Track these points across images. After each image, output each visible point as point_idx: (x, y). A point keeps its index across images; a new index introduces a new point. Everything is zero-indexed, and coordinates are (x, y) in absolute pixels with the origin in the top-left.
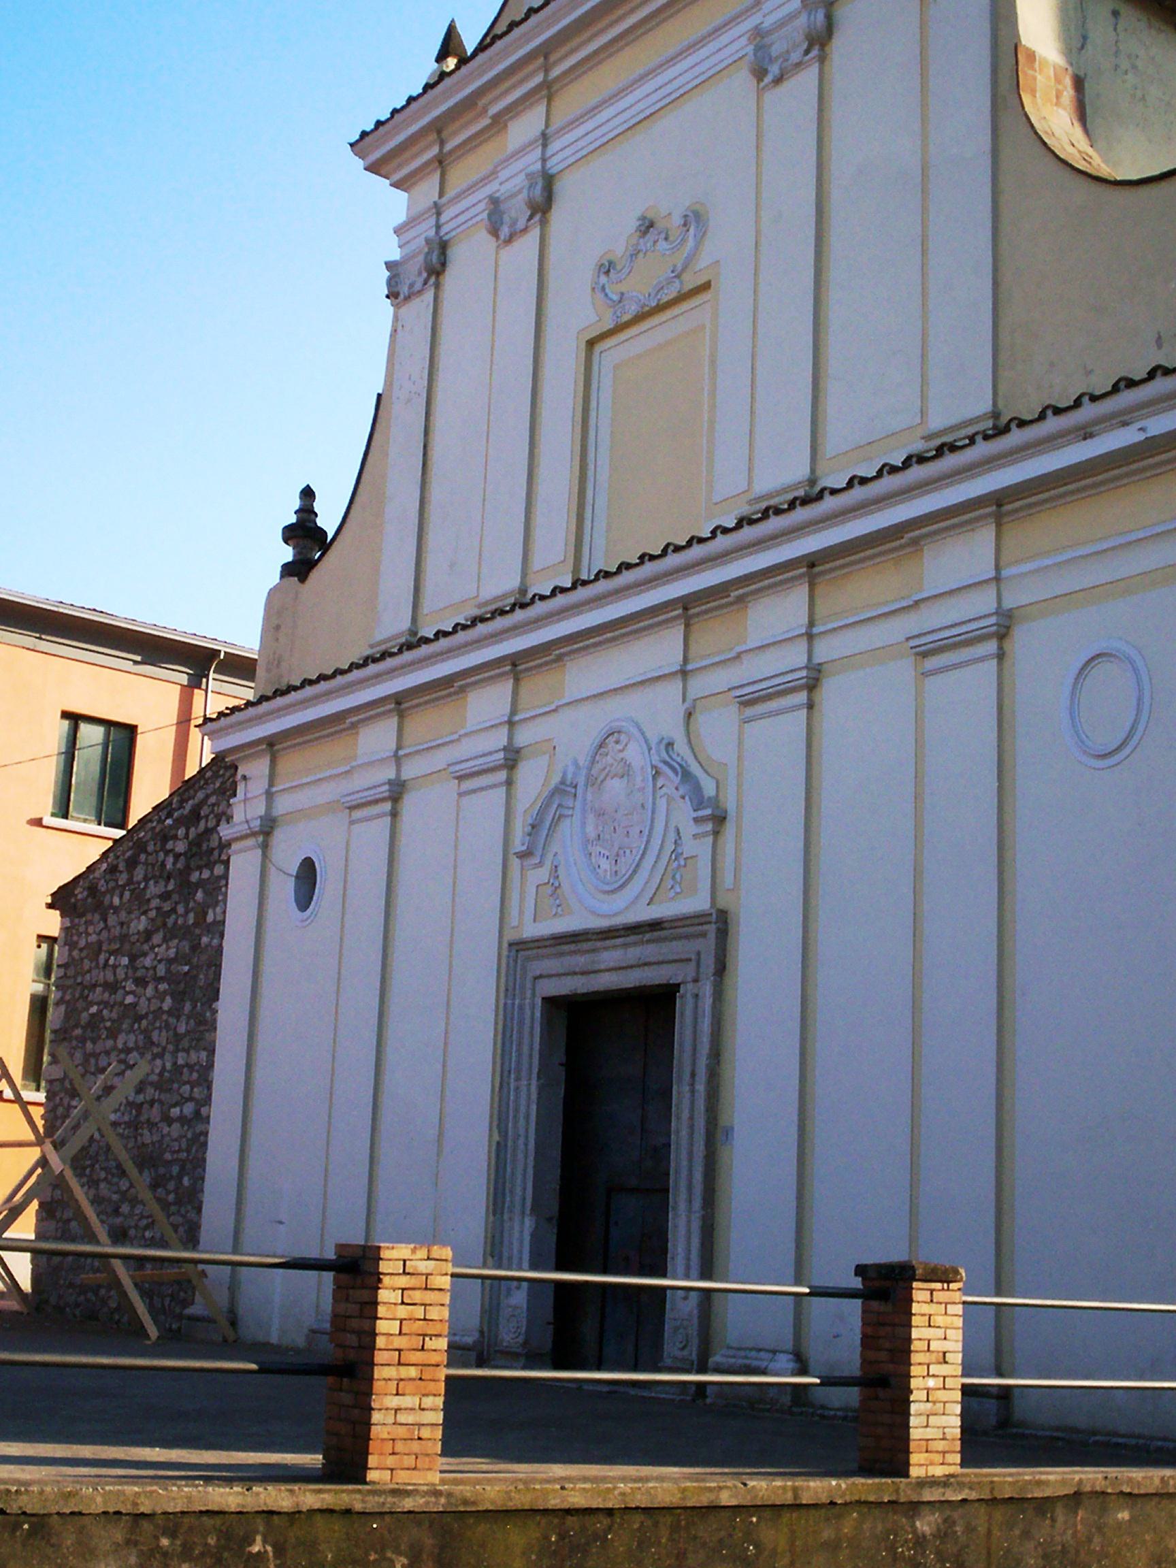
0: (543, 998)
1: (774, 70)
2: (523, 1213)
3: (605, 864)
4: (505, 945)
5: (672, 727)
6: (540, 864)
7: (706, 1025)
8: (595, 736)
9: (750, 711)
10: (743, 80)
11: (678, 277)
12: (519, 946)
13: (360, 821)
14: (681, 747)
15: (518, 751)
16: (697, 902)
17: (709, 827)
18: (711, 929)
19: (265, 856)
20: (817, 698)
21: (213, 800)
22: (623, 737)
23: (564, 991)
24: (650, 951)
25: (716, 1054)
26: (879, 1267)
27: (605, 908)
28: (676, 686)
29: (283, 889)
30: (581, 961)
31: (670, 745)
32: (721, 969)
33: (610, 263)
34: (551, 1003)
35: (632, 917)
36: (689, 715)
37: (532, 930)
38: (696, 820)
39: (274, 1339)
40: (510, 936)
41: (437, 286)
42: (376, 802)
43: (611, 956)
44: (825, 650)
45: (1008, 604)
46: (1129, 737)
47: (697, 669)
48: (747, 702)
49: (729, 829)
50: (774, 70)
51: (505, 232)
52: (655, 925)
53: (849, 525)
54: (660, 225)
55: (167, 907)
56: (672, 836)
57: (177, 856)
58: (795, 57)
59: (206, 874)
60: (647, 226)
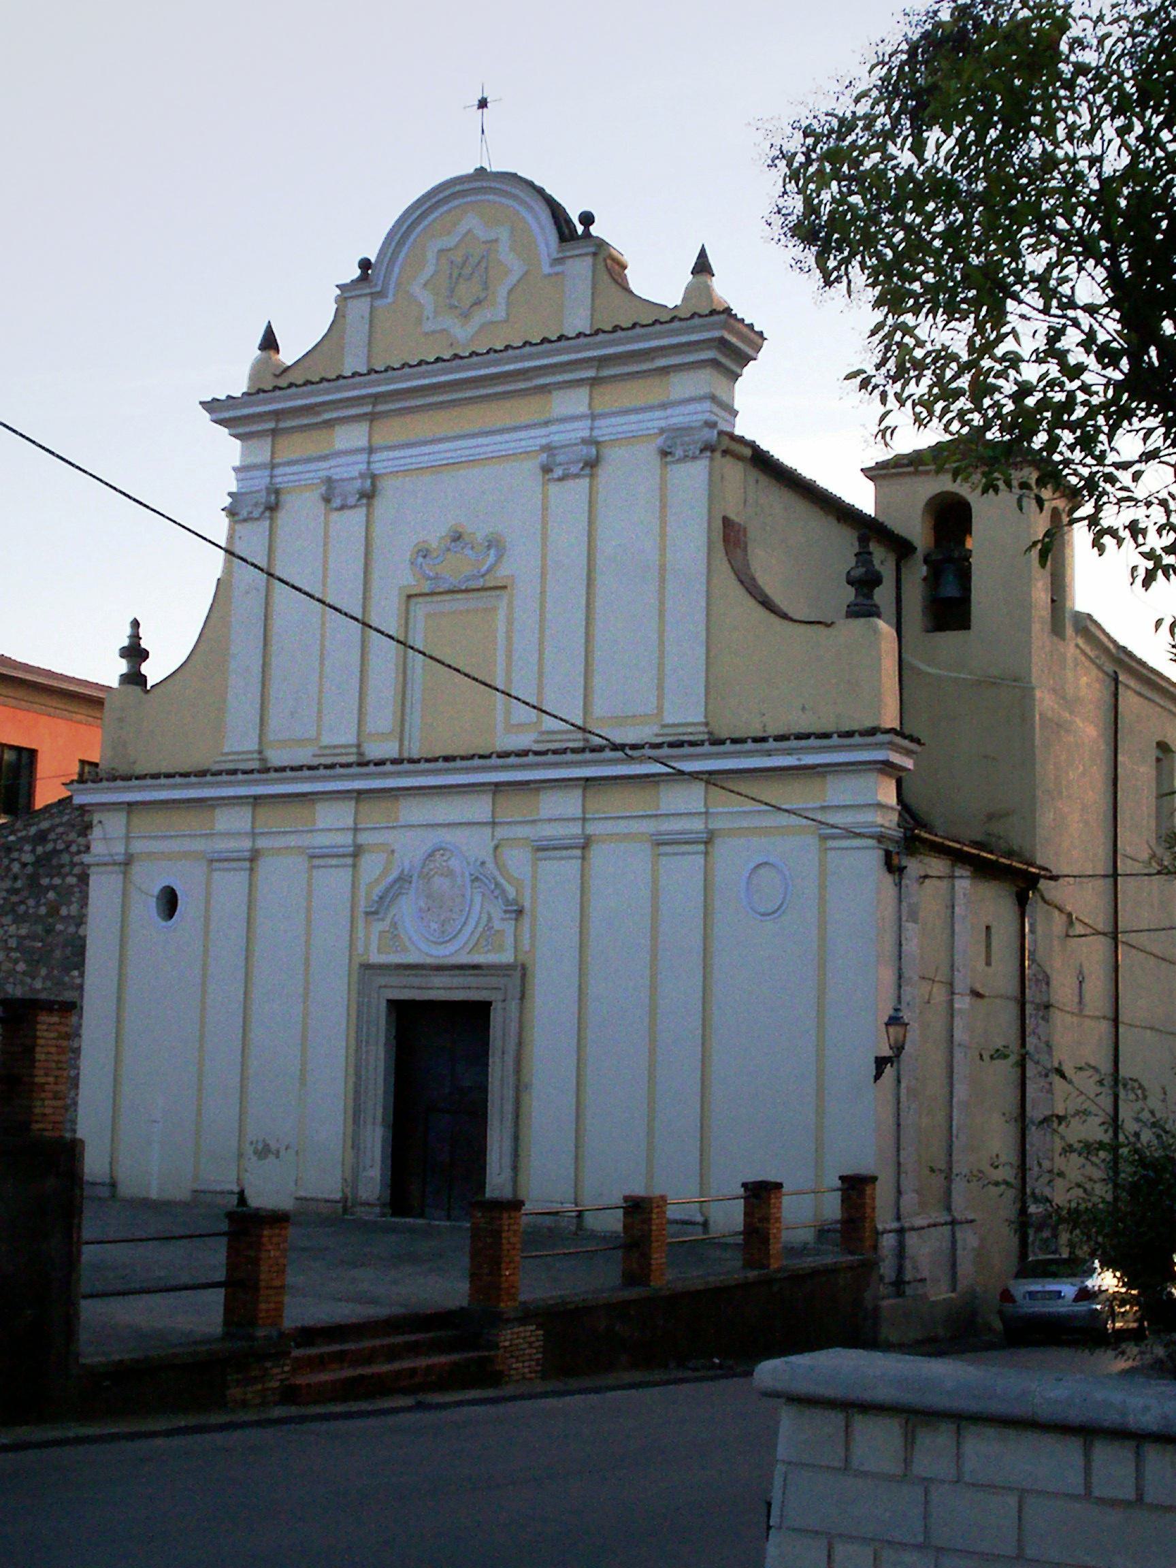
0: (389, 1001)
1: (558, 472)
2: (374, 1124)
3: (434, 926)
4: (356, 967)
5: (486, 854)
6: (383, 920)
7: (514, 1027)
8: (427, 847)
9: (541, 854)
10: (531, 467)
11: (483, 576)
12: (367, 967)
13: (319, 867)
14: (490, 865)
15: (132, 855)
16: (506, 957)
17: (513, 916)
18: (518, 974)
19: (125, 878)
20: (710, 849)
21: (60, 830)
22: (448, 854)
23: (402, 997)
24: (472, 981)
25: (520, 1044)
26: (755, 1183)
27: (435, 952)
28: (488, 831)
29: (146, 908)
30: (416, 981)
31: (483, 863)
32: (523, 997)
33: (427, 550)
34: (390, 1002)
35: (464, 959)
36: (496, 847)
37: (376, 958)
38: (506, 912)
39: (154, 1195)
40: (357, 960)
41: (271, 518)
42: (344, 856)
43: (438, 980)
44: (363, 838)
45: (710, 827)
46: (780, 906)
47: (717, 813)
48: (313, 857)
49: (526, 921)
50: (558, 472)
51: (337, 502)
52: (476, 967)
53: (456, 776)
54: (467, 539)
55: (14, 899)
56: (485, 917)
57: (24, 865)
58: (574, 469)
59: (57, 881)
60: (457, 537)
